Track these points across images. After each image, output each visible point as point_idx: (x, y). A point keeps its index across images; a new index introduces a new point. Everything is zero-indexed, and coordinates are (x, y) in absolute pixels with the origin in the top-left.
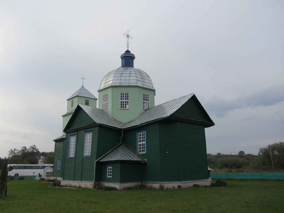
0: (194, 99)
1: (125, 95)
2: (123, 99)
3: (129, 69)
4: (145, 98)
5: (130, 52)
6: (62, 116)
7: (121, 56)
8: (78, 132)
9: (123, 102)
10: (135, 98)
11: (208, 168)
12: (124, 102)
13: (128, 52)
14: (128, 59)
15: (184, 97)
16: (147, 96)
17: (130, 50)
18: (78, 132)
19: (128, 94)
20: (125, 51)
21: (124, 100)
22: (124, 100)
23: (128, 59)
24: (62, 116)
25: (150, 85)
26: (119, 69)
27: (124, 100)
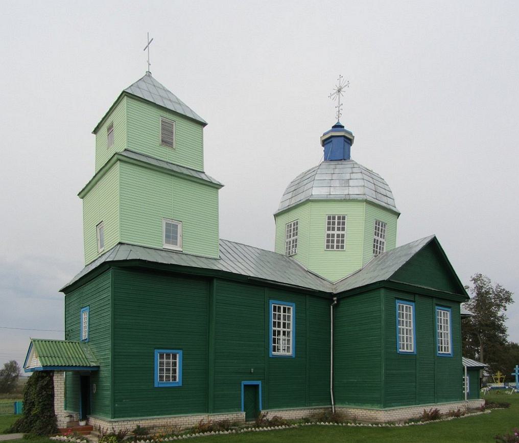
0: (433, 247)
1: (336, 221)
2: (333, 229)
3: (343, 169)
4: (379, 228)
5: (343, 127)
6: (223, 186)
7: (324, 135)
8: (15, 413)
9: (339, 229)
10: (358, 225)
11: (463, 358)
12: (334, 234)
13: (338, 127)
14: (338, 144)
15: (425, 238)
16: (384, 225)
17: (342, 123)
18: (15, 413)
19: (344, 218)
20: (333, 125)
21: (334, 230)
22: (334, 230)
23: (338, 144)
24: (223, 186)
25: (390, 201)
26: (233, 244)
27: (336, 232)
